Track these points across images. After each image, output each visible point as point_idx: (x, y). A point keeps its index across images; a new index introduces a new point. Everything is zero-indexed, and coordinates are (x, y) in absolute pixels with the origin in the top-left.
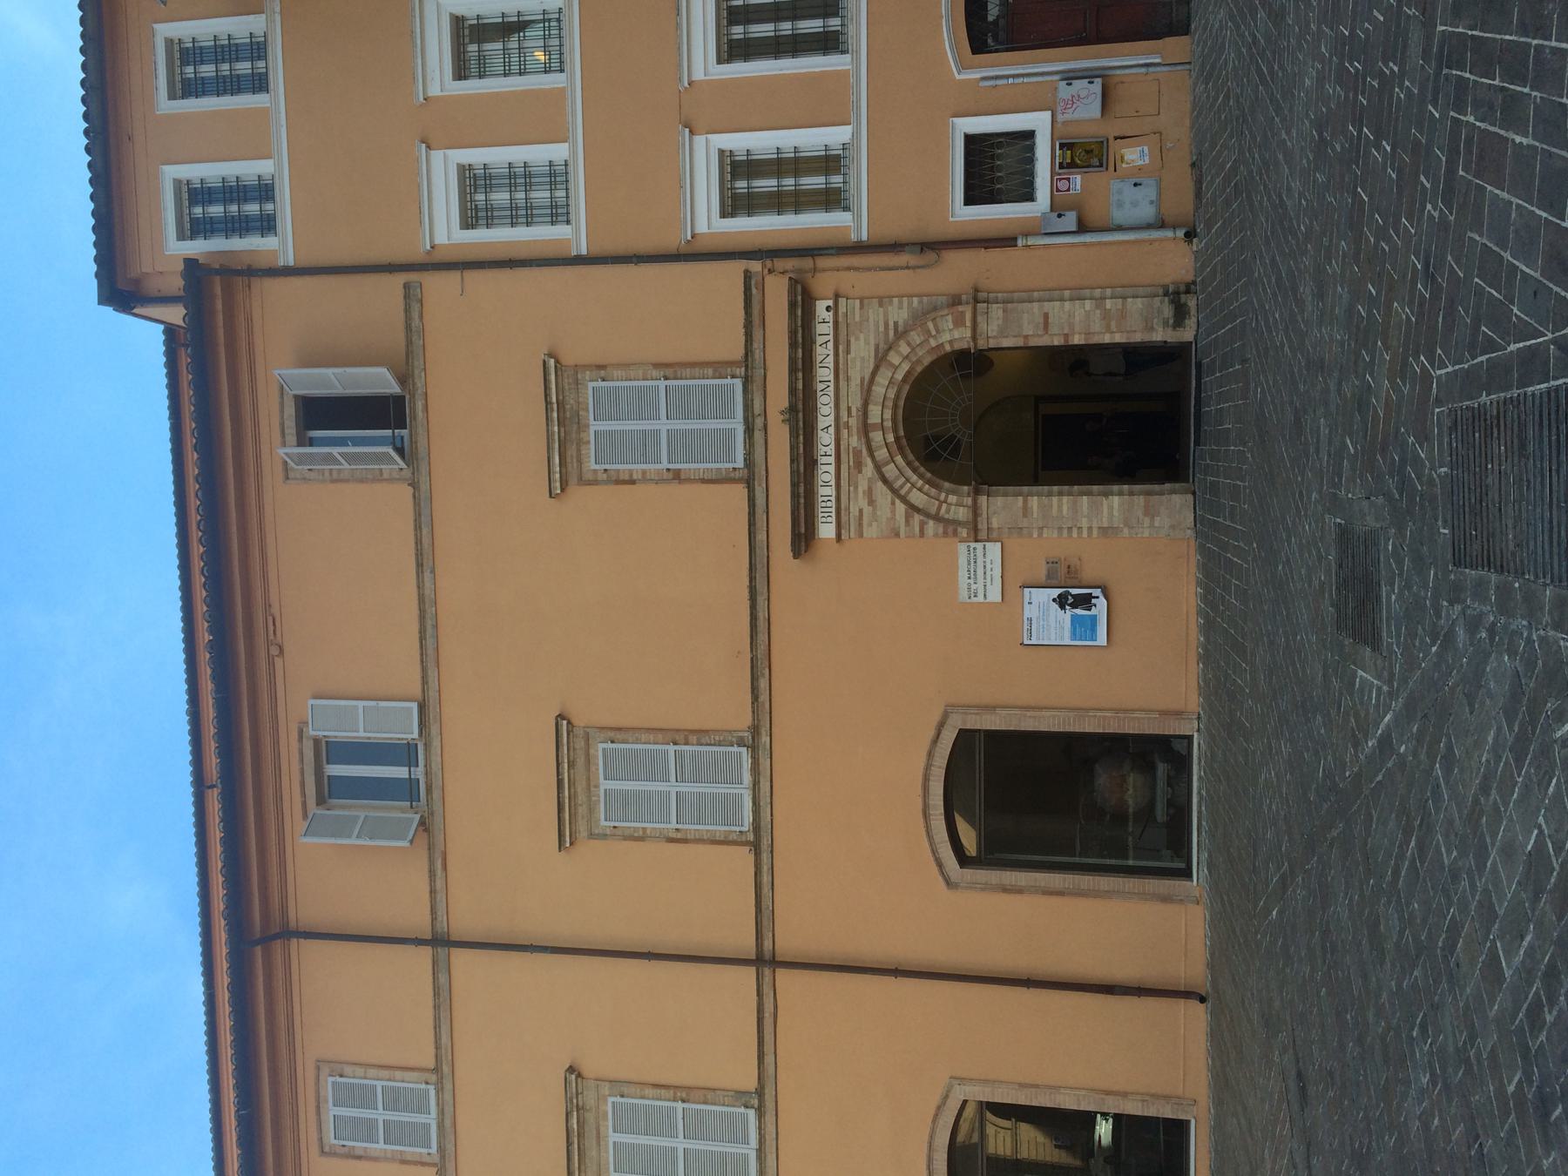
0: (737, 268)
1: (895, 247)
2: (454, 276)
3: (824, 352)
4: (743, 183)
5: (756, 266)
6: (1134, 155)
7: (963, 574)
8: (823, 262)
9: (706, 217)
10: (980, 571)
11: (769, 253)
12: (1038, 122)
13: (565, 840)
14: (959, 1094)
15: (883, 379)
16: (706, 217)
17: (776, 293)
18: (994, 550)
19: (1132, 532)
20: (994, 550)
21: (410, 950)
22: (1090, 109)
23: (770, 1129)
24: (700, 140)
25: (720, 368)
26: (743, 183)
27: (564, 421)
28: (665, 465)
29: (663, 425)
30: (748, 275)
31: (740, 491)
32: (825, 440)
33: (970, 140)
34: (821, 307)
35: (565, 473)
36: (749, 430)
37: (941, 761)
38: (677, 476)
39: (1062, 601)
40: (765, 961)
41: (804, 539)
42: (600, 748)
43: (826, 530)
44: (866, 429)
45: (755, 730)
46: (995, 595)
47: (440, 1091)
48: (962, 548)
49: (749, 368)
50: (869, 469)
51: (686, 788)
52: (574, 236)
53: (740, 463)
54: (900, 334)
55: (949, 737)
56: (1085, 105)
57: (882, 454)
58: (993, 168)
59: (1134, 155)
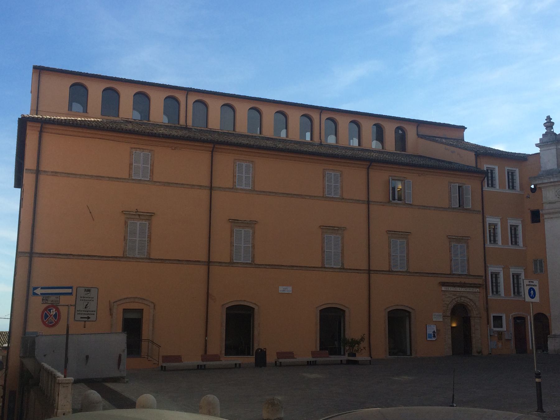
0: (483, 274)
1: (487, 303)
2: (481, 221)
3: (471, 290)
4: (495, 276)
5: (484, 278)
6: (500, 345)
7: (437, 314)
8: (484, 290)
9: (491, 269)
10: (438, 317)
11: (486, 280)
12: (504, 328)
13: (388, 232)
14: (256, 308)
15: (468, 300)
16: (491, 269)
17: (480, 281)
18: (441, 320)
19: (445, 346)
20: (441, 320)
21: (35, 165)
22: (507, 338)
23: (337, 270)
24: (523, 270)
25: (343, 264)
26: (495, 276)
27: (139, 215)
28: (453, 258)
29: (333, 251)
30: (482, 276)
31: (387, 269)
32: (458, 289)
33: (501, 317)
34: (478, 289)
35: (451, 239)
36: (459, 275)
37: (246, 304)
38: (451, 260)
39: (434, 332)
40: (209, 263)
41: (443, 284)
42: (147, 223)
43: (443, 288)
44: (461, 297)
45: (150, 259)
46: (434, 320)
47: (249, 190)
48: (441, 314)
49: (451, 274)
50: (454, 297)
51: (243, 247)
52: (488, 245)
53: (234, 261)
54: (475, 304)
55: (251, 305)
56: (506, 337)
57: (456, 299)
58: (498, 320)
59: (500, 345)
